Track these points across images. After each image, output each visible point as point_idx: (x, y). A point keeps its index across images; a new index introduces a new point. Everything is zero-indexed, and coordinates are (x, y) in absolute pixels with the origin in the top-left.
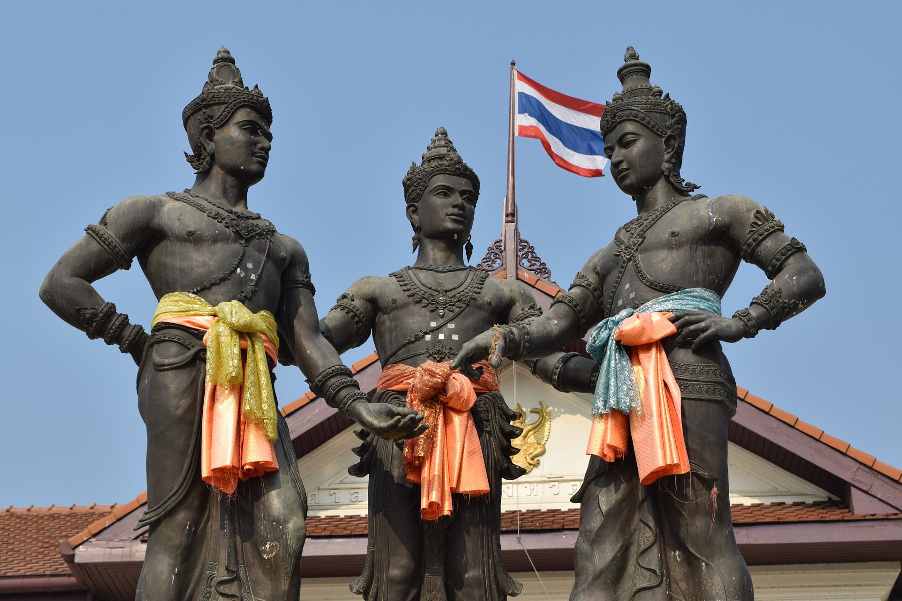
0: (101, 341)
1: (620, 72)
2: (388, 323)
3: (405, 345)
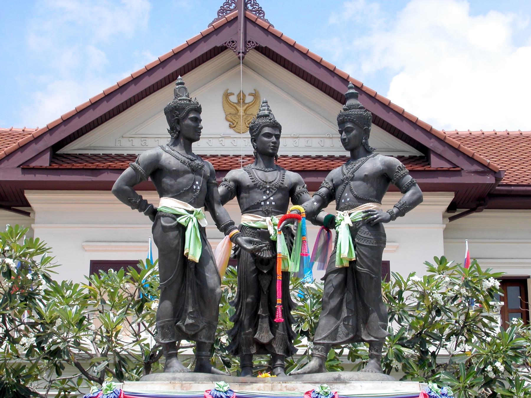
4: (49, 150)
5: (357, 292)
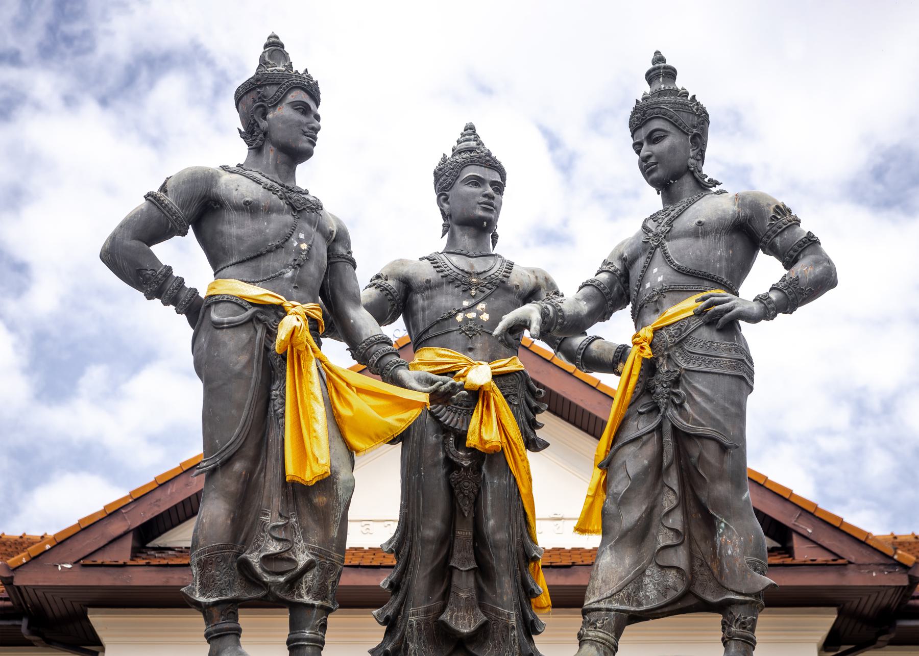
0: (157, 301)
1: (648, 74)
2: (421, 302)
3: (438, 322)
4: (130, 538)
5: (688, 488)
